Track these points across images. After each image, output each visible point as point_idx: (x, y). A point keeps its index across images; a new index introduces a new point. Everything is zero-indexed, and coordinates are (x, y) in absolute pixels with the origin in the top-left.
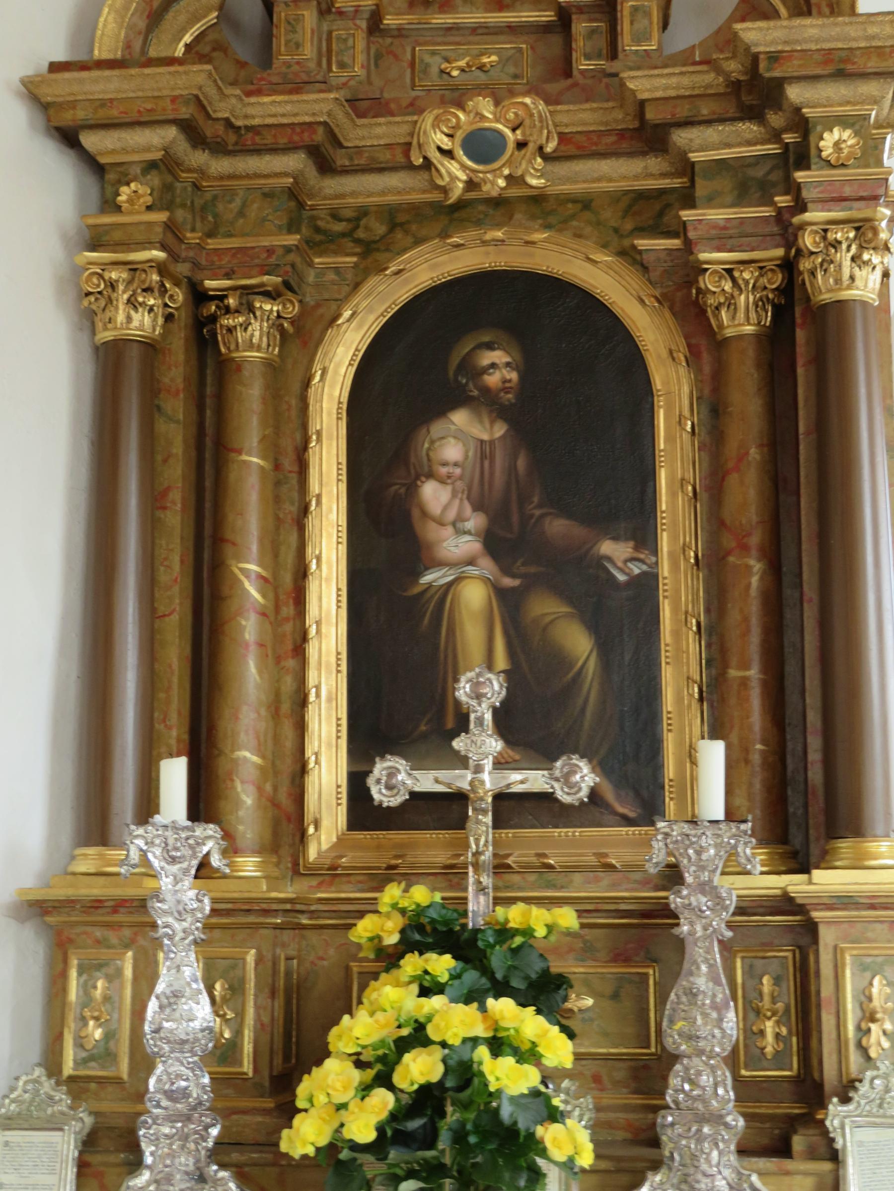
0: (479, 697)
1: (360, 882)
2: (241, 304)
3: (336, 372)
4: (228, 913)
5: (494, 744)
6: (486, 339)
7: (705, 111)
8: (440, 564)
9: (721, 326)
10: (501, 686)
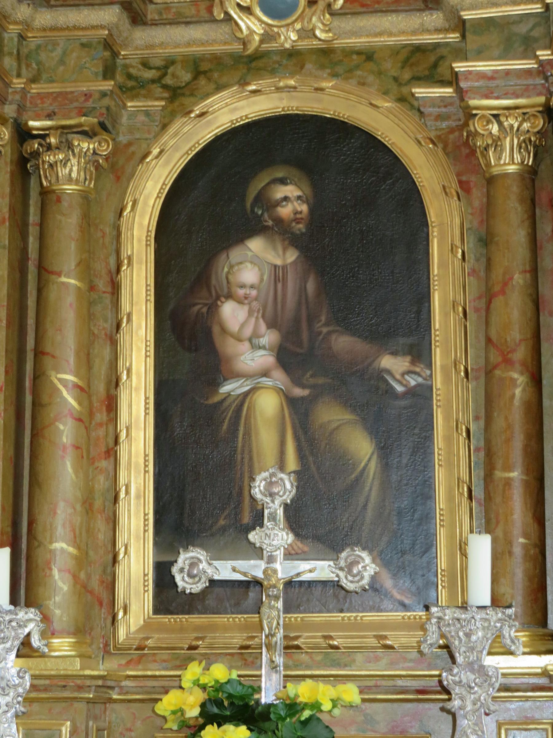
3: (146, 203)
5: (285, 537)
8: (238, 375)
10: (292, 487)
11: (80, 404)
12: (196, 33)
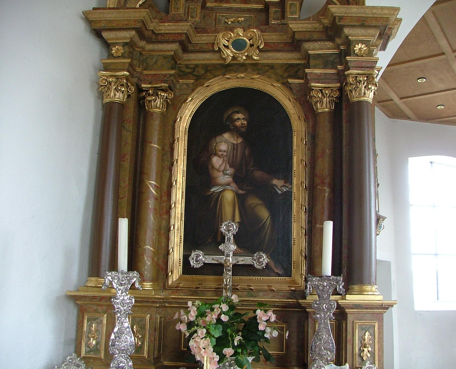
0: (229, 231)
1: (186, 292)
2: (154, 93)
3: (185, 119)
4: (141, 302)
5: (233, 247)
6: (236, 110)
7: (315, 36)
8: (218, 185)
9: (317, 109)
10: (236, 227)
11: (157, 193)
12: (208, 56)
